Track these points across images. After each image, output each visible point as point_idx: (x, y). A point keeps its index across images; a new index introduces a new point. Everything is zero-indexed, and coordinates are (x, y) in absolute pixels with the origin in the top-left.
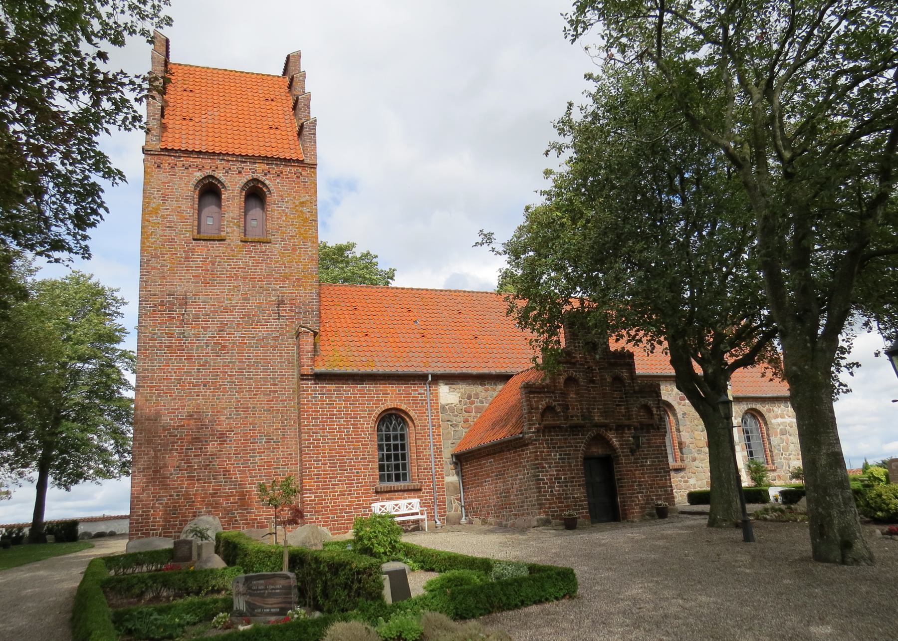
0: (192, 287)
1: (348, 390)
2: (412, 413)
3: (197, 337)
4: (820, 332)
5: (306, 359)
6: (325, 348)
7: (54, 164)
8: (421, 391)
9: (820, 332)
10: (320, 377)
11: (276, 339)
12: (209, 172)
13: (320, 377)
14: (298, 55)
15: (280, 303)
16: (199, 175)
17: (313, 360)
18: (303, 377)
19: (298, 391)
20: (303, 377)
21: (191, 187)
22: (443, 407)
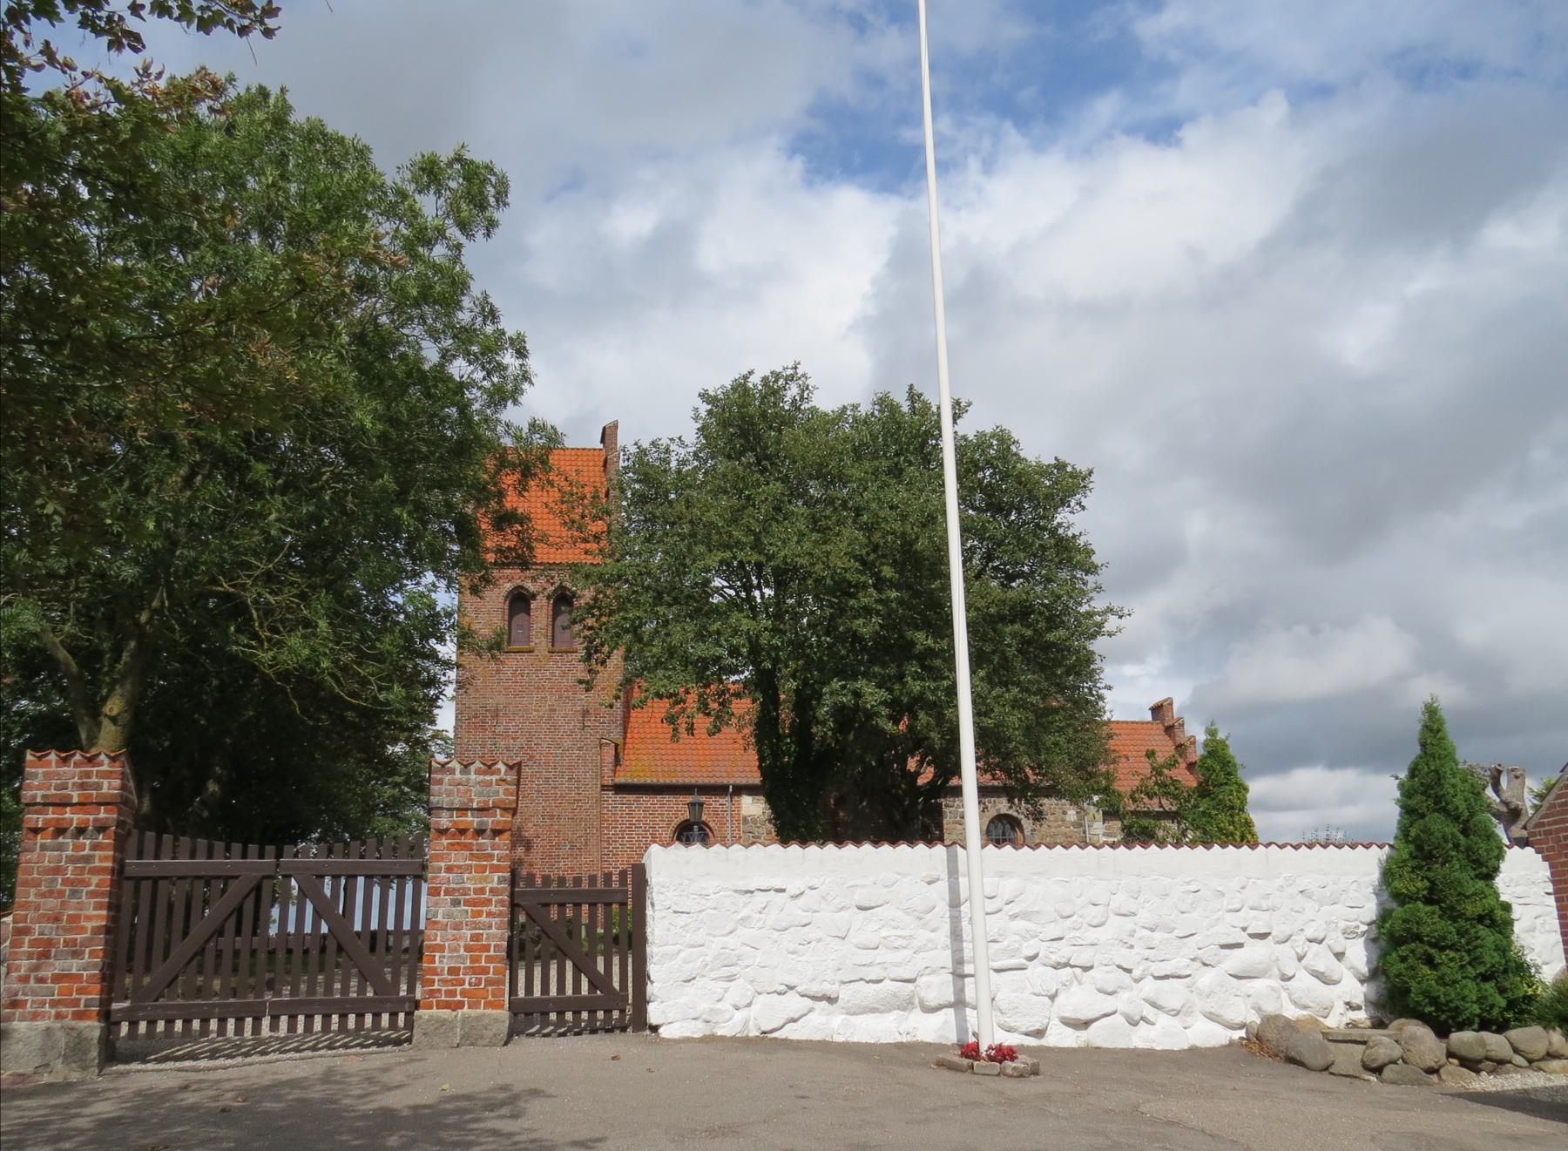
0: (502, 699)
1: (647, 800)
2: (712, 824)
3: (508, 749)
4: (133, 644)
5: (608, 770)
6: (628, 757)
7: (257, 482)
8: (722, 801)
9: (133, 644)
10: (620, 789)
11: (580, 749)
12: (519, 582)
13: (620, 789)
14: (615, 426)
15: (585, 713)
16: (508, 586)
17: (615, 772)
18: (604, 788)
19: (600, 801)
20: (604, 788)
21: (501, 599)
22: (745, 819)
